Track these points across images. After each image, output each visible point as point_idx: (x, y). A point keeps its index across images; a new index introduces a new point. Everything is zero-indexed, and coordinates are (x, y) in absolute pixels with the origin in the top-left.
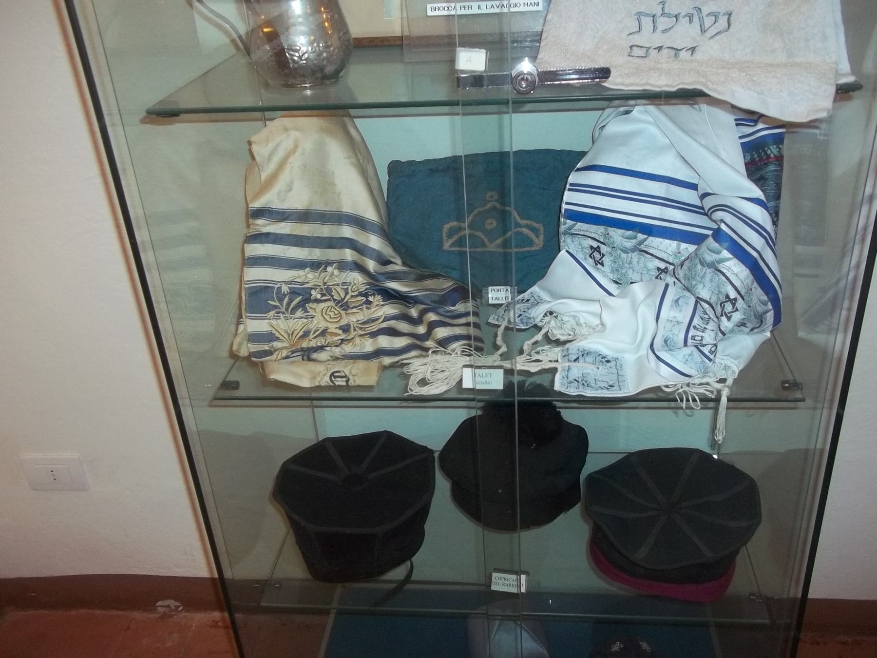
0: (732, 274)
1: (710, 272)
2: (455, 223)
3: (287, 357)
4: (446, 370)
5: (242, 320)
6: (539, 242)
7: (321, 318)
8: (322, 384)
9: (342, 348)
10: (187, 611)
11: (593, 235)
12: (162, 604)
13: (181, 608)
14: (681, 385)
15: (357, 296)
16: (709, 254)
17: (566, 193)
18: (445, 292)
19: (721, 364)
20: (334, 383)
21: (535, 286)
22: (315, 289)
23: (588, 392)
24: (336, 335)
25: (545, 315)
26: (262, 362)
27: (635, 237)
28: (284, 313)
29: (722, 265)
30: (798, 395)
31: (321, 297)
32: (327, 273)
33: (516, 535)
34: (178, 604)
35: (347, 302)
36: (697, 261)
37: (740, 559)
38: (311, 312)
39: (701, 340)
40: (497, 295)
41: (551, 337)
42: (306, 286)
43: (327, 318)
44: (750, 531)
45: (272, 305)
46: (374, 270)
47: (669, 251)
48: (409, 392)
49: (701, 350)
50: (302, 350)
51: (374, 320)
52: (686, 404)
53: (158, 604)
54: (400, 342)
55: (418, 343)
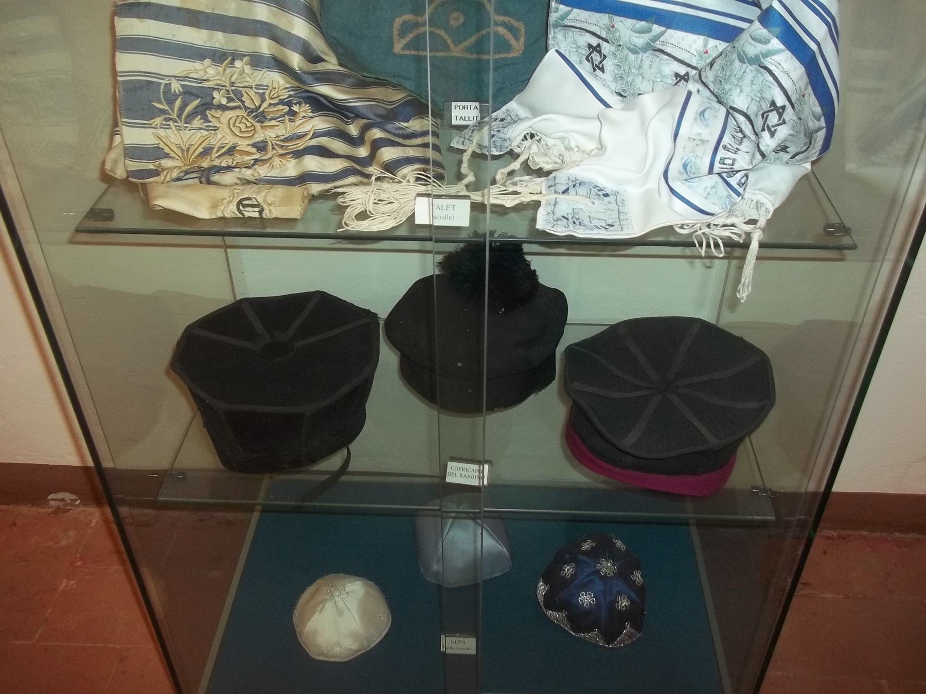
0: (782, 71)
1: (751, 71)
2: (408, 17)
3: (179, 179)
5: (118, 129)
6: (518, 46)
7: (228, 131)
8: (226, 215)
9: (255, 169)
10: (86, 505)
13: (78, 502)
14: (699, 225)
15: (276, 105)
16: (752, 45)
18: (395, 106)
19: (752, 200)
20: (242, 214)
21: (512, 102)
22: (219, 90)
24: (248, 153)
26: (144, 184)
27: (649, 31)
28: (175, 121)
29: (769, 59)
30: (846, 241)
32: (235, 69)
33: (479, 420)
34: (74, 497)
35: (263, 112)
36: (735, 55)
38: (214, 123)
39: (732, 165)
41: (532, 167)
42: (205, 84)
44: (759, 416)
45: (158, 108)
46: (298, 67)
48: (344, 228)
49: (727, 181)
50: (200, 170)
52: (706, 251)
53: (50, 497)
54: (332, 166)
55: (358, 168)
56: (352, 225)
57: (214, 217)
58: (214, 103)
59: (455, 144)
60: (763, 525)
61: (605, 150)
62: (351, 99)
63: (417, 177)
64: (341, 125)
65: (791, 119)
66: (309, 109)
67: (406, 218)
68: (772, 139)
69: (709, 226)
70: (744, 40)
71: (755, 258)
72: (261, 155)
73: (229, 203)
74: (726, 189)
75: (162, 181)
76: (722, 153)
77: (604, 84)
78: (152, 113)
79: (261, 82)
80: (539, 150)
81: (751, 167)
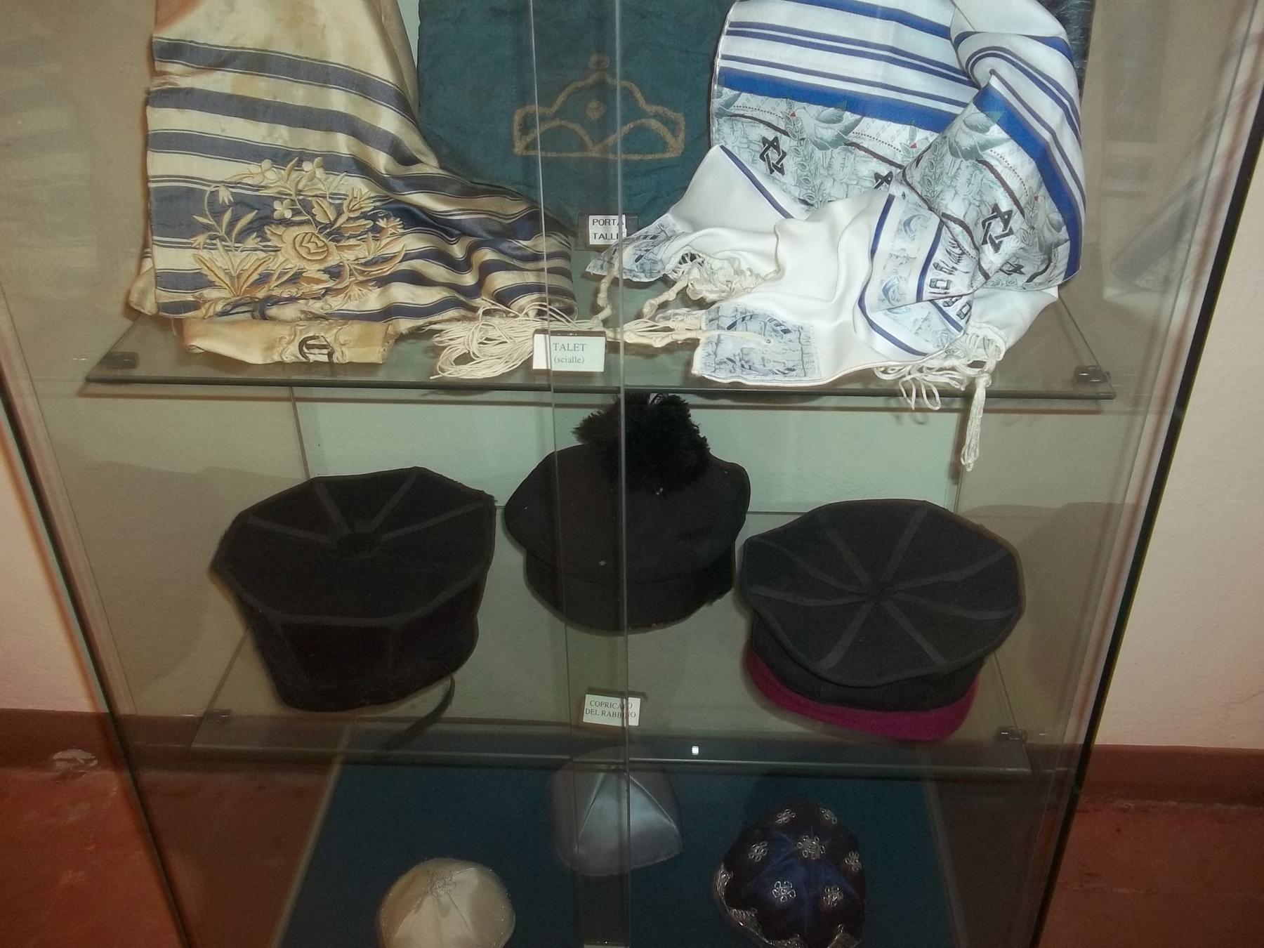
0: (1006, 167)
3: (225, 313)
4: (507, 341)
5: (149, 250)
6: (676, 145)
8: (285, 359)
9: (326, 301)
11: (767, 118)
12: (61, 757)
13: (95, 762)
14: (908, 368)
16: (967, 133)
17: (724, 40)
19: (978, 336)
20: (306, 357)
21: (666, 215)
22: (281, 200)
23: (750, 379)
24: (318, 281)
25: (683, 260)
27: (839, 120)
28: (223, 240)
29: (988, 151)
30: (1102, 389)
31: (293, 216)
34: (89, 756)
35: (339, 228)
36: (946, 148)
37: (985, 673)
38: (274, 242)
39: (947, 288)
40: (599, 229)
41: (691, 297)
42: (263, 193)
43: (303, 252)
44: (1005, 626)
45: (201, 223)
46: (386, 170)
47: (896, 144)
48: (439, 374)
51: (386, 260)
52: (916, 402)
55: (462, 298)
56: (449, 370)
57: (269, 361)
58: (275, 217)
59: (593, 268)
60: (1015, 780)
61: (784, 272)
62: (454, 210)
63: (539, 310)
64: (441, 244)
65: (1020, 228)
66: (400, 225)
67: (521, 362)
68: (996, 254)
69: (921, 370)
70: (957, 127)
71: (982, 410)
72: (335, 283)
73: (289, 343)
74: (942, 321)
75: (202, 316)
76: (933, 273)
77: (784, 190)
78: (193, 229)
79: (339, 190)
80: (702, 275)
81: (971, 291)
